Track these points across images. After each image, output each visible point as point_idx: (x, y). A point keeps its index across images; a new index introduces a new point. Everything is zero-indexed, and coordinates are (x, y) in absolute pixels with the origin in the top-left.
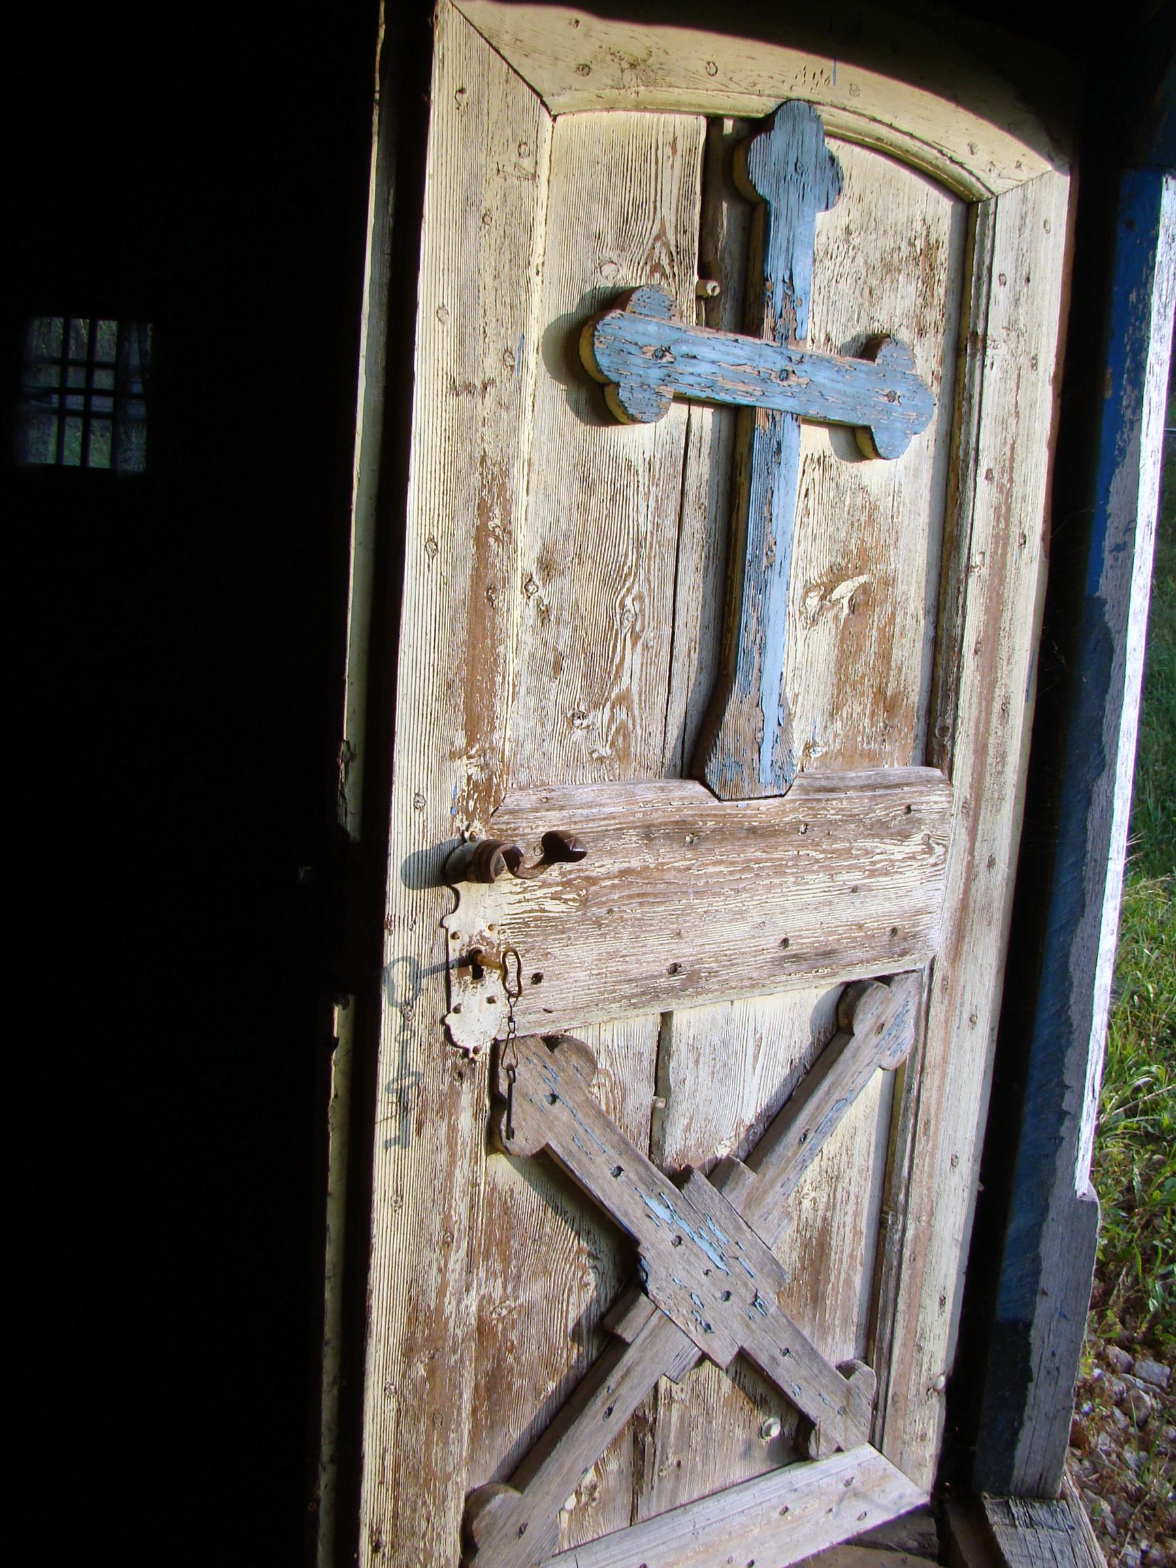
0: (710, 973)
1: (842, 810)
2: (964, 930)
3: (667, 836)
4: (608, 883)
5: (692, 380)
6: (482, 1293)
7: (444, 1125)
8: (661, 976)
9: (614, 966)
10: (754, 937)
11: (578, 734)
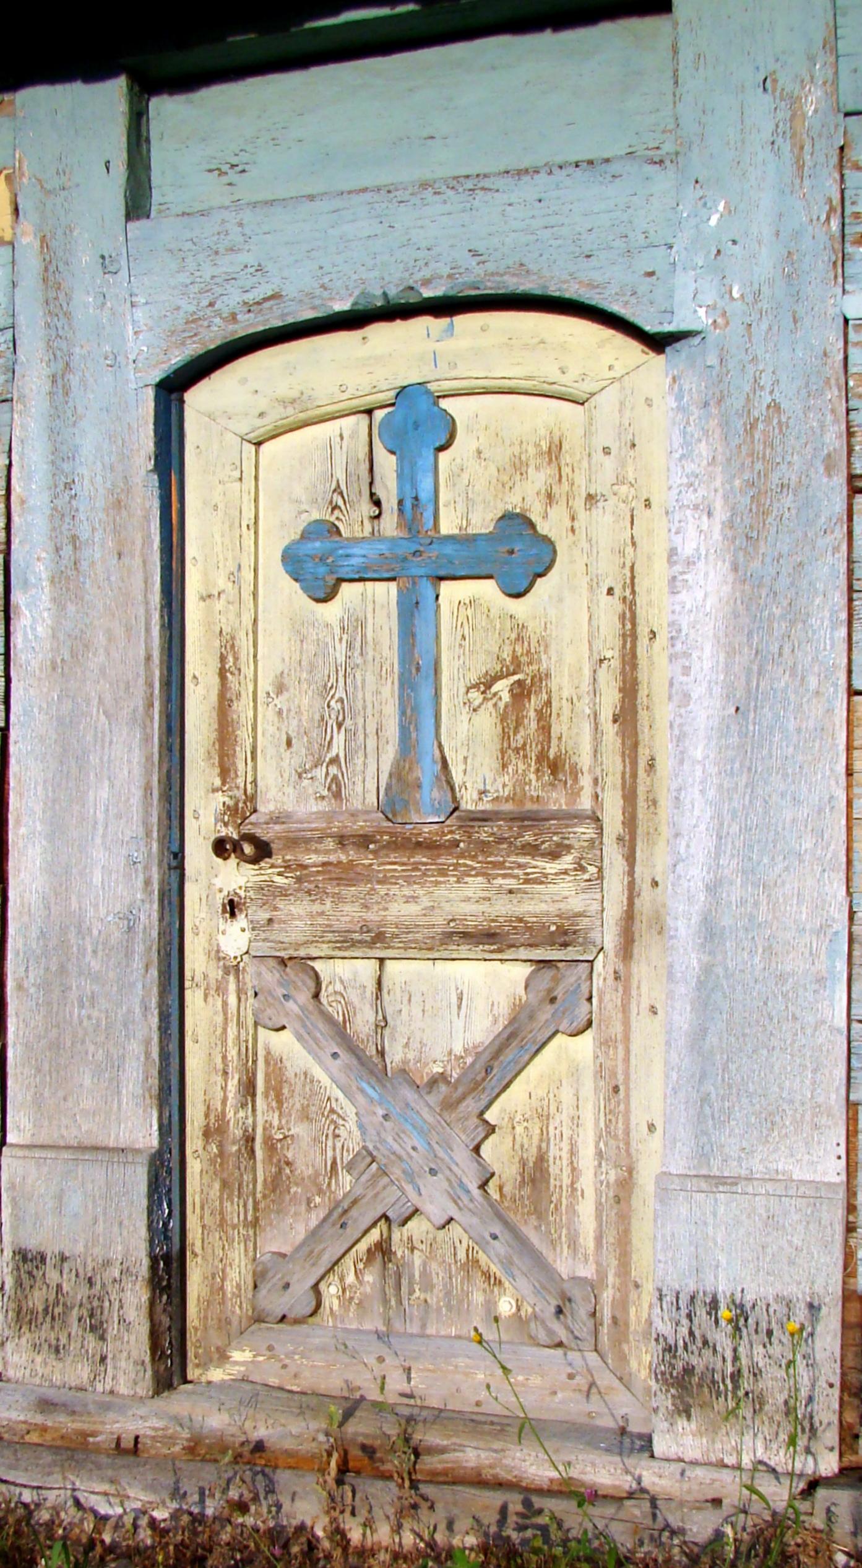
1: (493, 834)
3: (354, 843)
4: (314, 869)
5: (347, 569)
8: (355, 932)
9: (320, 921)
10: (425, 915)
11: (306, 782)
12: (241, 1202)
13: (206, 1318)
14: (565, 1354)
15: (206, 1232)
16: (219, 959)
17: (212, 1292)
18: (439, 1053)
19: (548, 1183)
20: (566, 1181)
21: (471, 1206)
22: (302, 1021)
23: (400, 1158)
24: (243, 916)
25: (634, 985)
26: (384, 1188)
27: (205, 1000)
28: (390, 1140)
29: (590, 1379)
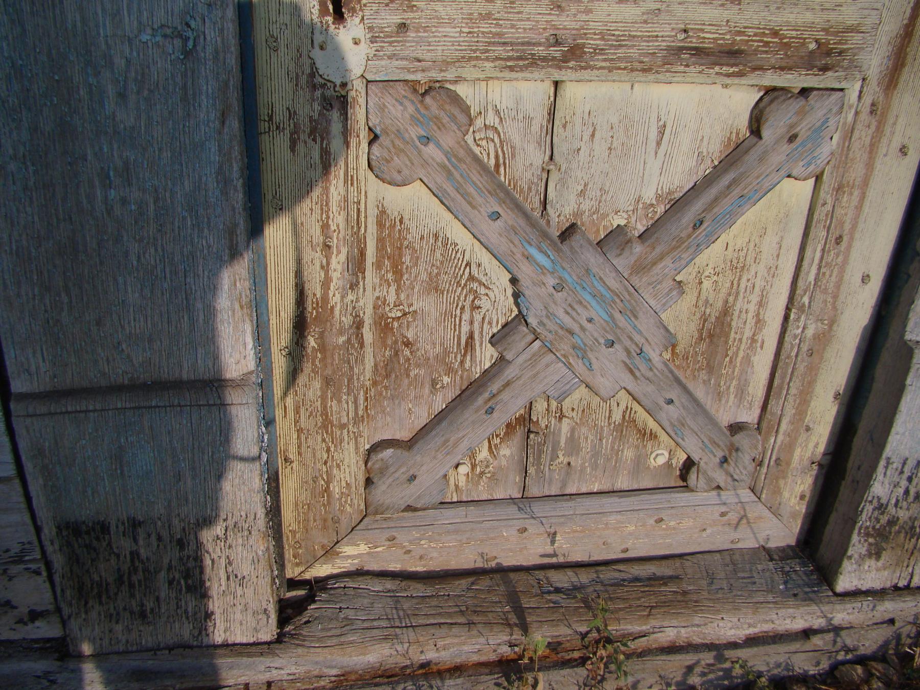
0: (595, 50)
2: (905, 58)
6: (377, 294)
7: (317, 147)
8: (540, 44)
9: (485, 27)
10: (645, 22)
12: (351, 398)
13: (306, 520)
14: (719, 495)
15: (303, 437)
16: (314, 87)
17: (313, 495)
18: (624, 201)
19: (727, 336)
20: (748, 333)
21: (649, 374)
22: (449, 173)
23: (571, 332)
24: (357, 20)
25: (891, 121)
26: (547, 366)
27: (293, 148)
28: (560, 313)
29: (742, 513)
